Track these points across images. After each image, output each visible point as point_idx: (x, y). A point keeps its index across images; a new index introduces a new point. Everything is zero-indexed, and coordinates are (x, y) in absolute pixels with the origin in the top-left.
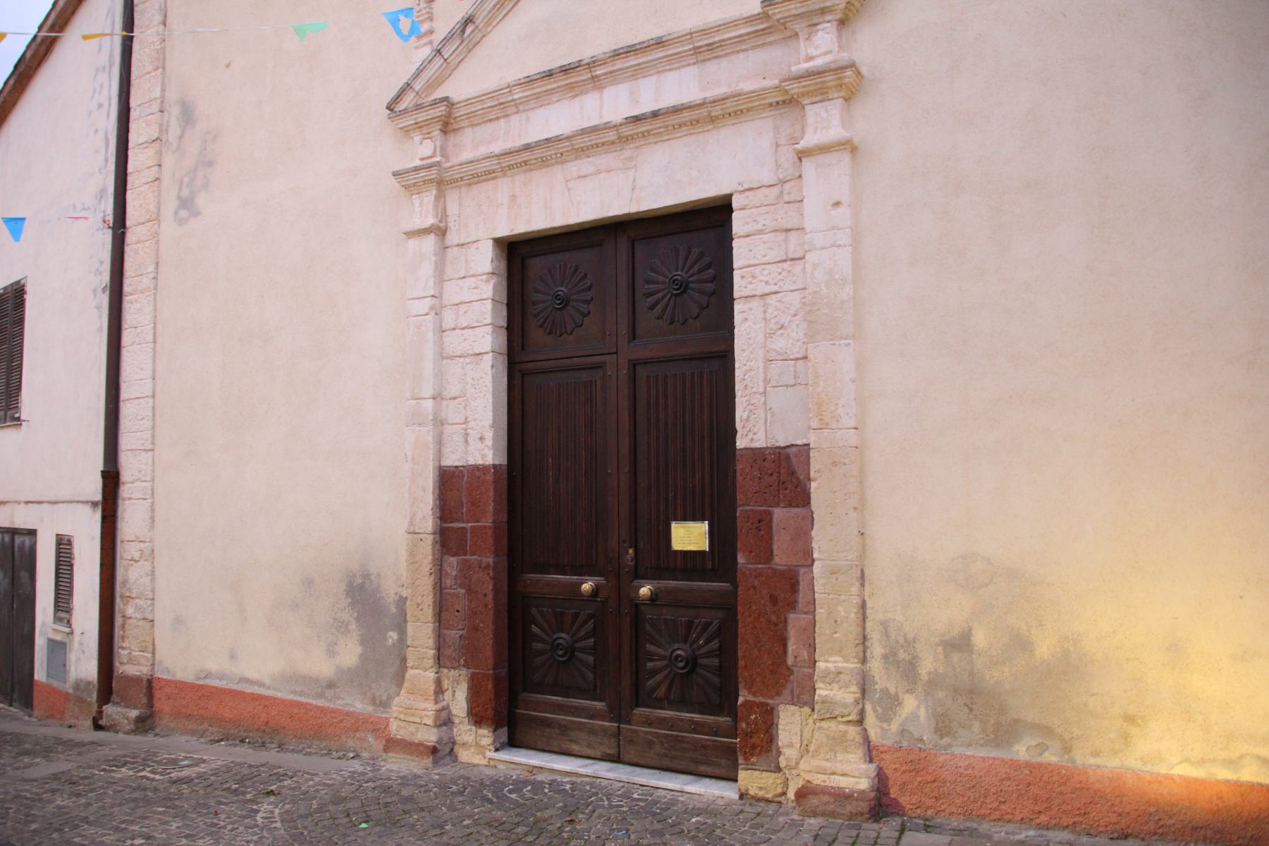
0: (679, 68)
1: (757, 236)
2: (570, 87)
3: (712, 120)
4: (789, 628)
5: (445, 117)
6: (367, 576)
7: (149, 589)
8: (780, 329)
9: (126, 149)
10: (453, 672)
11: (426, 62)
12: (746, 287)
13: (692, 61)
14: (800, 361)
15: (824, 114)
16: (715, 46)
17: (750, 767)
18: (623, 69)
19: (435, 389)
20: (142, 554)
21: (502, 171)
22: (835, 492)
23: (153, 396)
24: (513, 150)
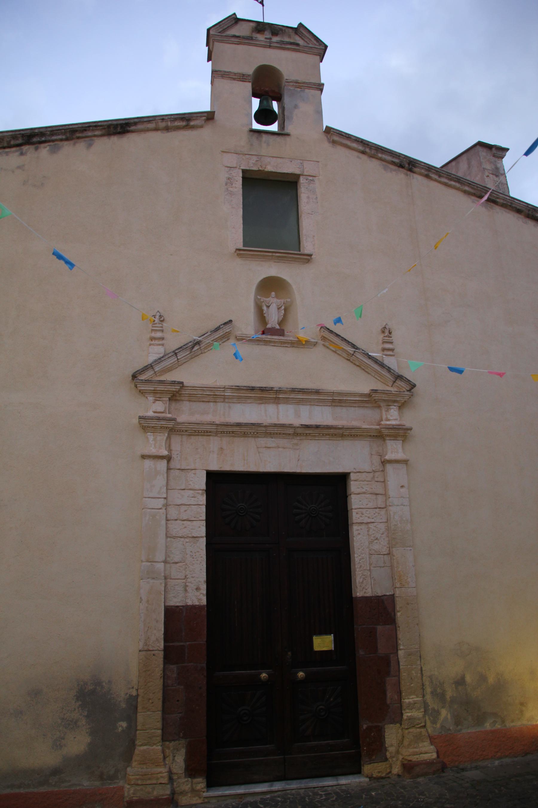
2: (261, 398)
4: (387, 685)
6: (98, 683)
8: (376, 540)
10: (173, 743)
12: (359, 518)
14: (386, 556)
15: (395, 446)
16: (342, 401)
17: (372, 762)
24: (229, 424)
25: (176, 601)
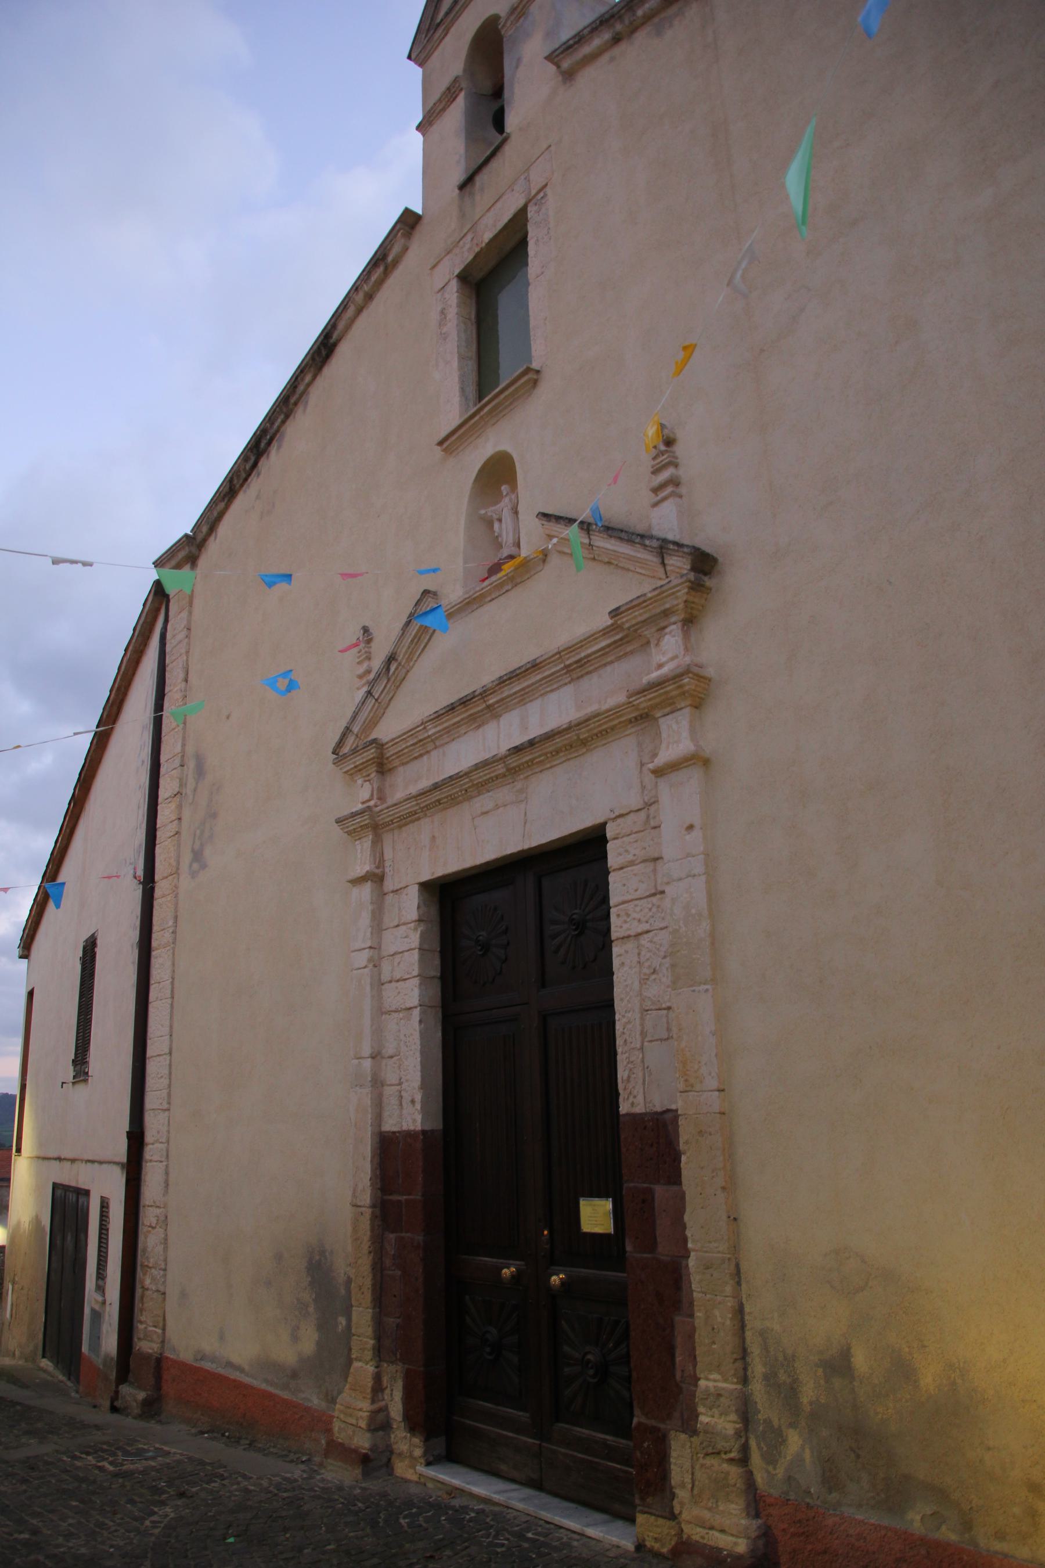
0: (557, 688)
1: (629, 868)
3: (584, 743)
4: (676, 1334)
5: (378, 758)
6: (322, 1253)
7: (162, 1258)
9: (156, 804)
11: (360, 705)
12: (621, 927)
13: (567, 681)
15: (675, 727)
16: (583, 662)
17: (646, 1509)
18: (511, 695)
19: (372, 1047)
20: (158, 1220)
21: (422, 811)
22: (702, 1168)
23: (170, 1053)
25: (390, 1125)
